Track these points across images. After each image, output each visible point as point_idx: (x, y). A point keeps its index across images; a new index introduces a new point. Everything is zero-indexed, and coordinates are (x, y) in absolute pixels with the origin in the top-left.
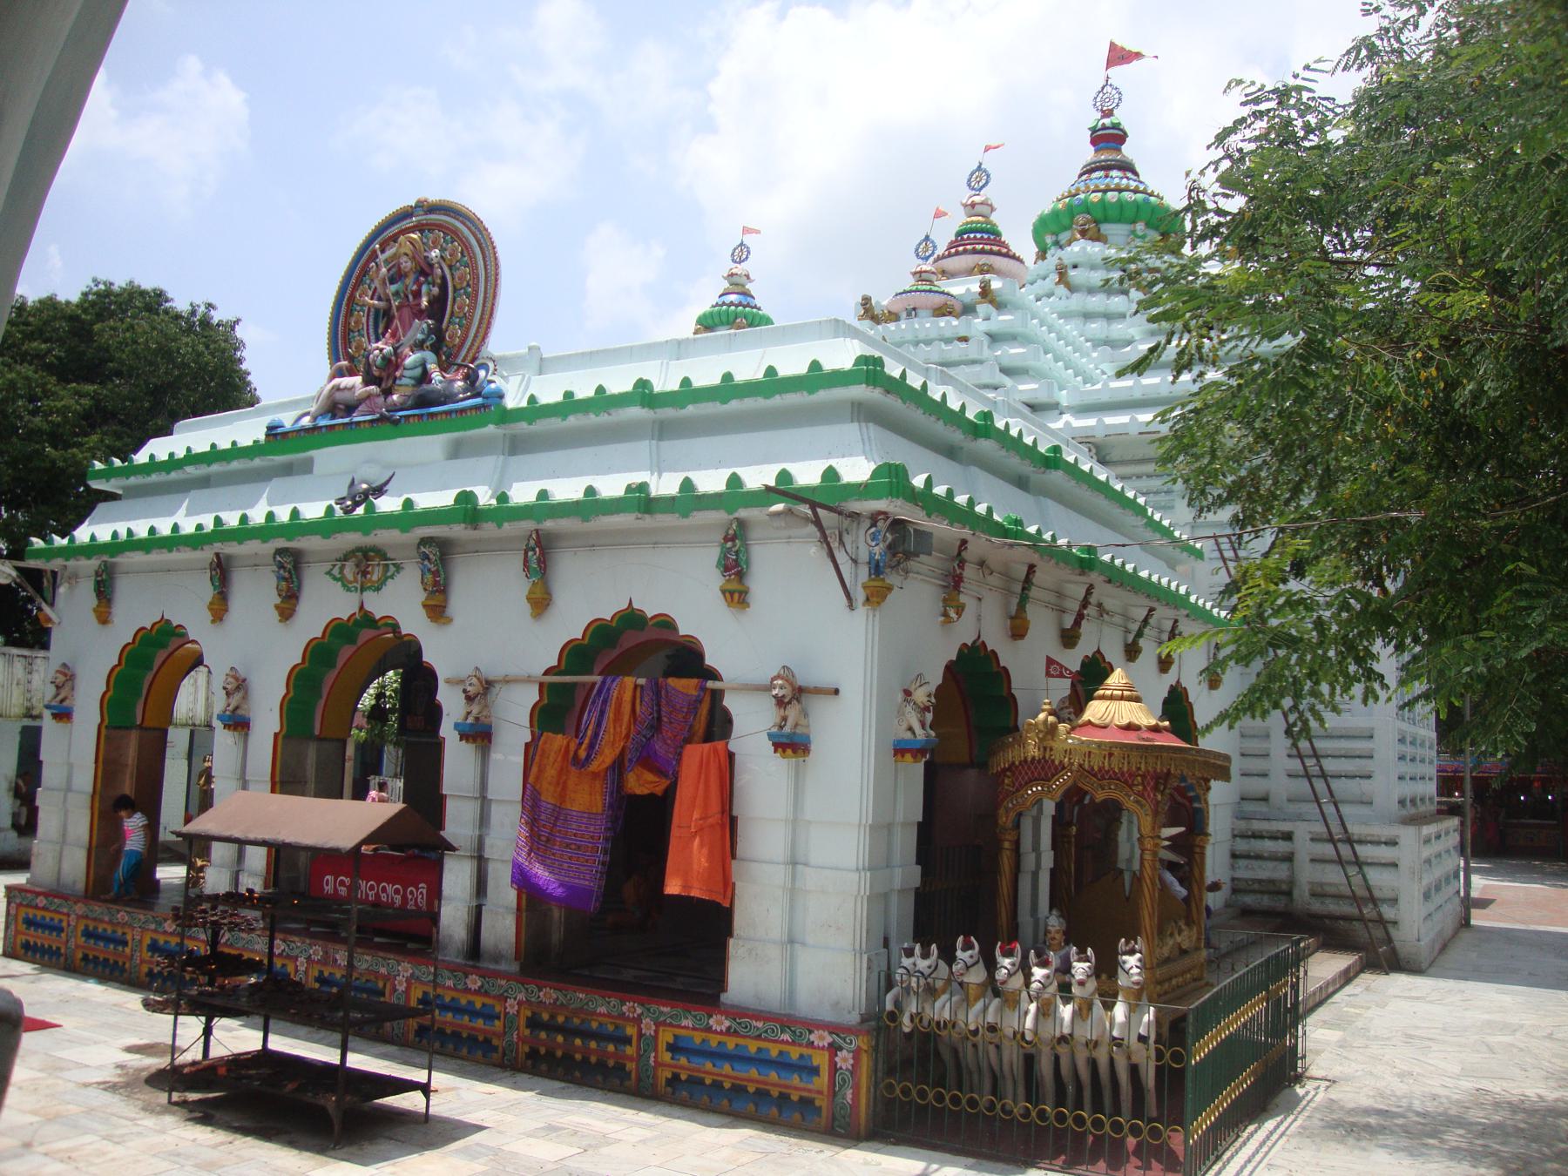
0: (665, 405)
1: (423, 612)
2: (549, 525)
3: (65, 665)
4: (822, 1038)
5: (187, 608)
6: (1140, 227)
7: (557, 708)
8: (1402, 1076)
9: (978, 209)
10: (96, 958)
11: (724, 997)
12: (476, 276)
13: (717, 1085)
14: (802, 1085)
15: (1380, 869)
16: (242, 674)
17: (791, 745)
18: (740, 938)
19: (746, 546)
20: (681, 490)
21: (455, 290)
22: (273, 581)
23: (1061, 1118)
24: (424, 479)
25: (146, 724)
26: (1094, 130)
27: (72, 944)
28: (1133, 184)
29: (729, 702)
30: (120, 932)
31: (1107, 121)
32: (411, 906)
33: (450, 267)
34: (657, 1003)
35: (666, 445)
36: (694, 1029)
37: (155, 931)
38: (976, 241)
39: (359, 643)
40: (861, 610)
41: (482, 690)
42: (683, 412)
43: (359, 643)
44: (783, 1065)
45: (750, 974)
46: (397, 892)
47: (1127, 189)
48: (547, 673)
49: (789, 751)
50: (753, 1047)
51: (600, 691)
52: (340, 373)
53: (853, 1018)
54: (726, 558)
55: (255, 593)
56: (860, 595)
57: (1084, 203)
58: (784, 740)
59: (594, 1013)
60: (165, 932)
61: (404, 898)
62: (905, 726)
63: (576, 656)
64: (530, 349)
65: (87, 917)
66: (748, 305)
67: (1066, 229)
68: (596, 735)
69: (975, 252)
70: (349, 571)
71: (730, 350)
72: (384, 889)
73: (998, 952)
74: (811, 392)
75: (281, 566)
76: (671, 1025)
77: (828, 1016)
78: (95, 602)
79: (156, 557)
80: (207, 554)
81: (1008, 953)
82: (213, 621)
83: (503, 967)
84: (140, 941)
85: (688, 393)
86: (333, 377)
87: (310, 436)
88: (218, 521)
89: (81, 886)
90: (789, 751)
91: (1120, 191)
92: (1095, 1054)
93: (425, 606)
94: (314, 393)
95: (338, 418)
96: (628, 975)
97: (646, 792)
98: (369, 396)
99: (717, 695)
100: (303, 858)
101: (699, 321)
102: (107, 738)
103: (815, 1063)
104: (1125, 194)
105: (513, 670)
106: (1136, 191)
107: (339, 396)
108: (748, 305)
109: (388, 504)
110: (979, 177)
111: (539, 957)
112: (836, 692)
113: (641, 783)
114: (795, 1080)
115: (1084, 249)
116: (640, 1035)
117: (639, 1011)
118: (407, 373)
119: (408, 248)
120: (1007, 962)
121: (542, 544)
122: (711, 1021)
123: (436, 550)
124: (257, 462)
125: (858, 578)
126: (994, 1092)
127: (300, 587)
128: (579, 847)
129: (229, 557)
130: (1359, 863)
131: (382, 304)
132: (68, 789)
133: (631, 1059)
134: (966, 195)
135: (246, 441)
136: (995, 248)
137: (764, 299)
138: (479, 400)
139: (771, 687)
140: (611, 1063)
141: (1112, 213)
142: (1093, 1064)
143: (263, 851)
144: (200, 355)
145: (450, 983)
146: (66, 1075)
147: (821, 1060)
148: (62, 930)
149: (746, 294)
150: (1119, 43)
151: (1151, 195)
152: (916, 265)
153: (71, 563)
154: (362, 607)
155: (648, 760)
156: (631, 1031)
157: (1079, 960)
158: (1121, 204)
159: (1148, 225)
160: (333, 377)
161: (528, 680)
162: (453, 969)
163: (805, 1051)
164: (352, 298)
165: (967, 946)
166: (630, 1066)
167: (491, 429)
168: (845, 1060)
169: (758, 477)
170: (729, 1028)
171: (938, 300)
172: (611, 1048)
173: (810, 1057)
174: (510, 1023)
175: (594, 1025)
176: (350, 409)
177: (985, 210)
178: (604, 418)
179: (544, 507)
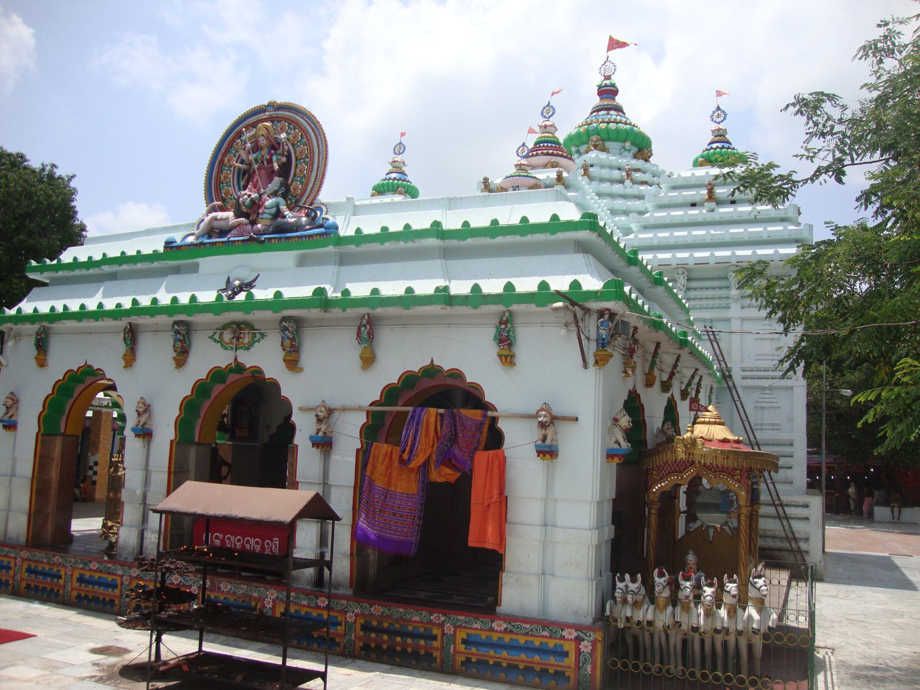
0: (449, 238)
1: (283, 364)
2: (379, 310)
3: (12, 393)
4: (570, 634)
5: (106, 357)
6: (628, 144)
7: (381, 426)
8: (867, 644)
9: (548, 129)
10: (36, 587)
11: (498, 609)
12: (312, 152)
13: (544, 672)
14: (557, 663)
15: (798, 521)
16: (148, 402)
17: (547, 452)
18: (510, 572)
19: (513, 327)
20: (472, 292)
21: (297, 159)
22: (171, 342)
23: (704, 676)
24: (282, 279)
26: (600, 87)
27: (18, 577)
28: (624, 120)
29: (501, 425)
30: (55, 569)
31: (608, 82)
32: (267, 552)
33: (293, 145)
34: (455, 614)
35: (450, 263)
36: (482, 630)
37: (83, 569)
38: (547, 148)
39: (227, 383)
40: (592, 369)
41: (326, 415)
42: (464, 243)
43: (227, 383)
44: (542, 651)
45: (516, 594)
46: (257, 543)
47: (620, 122)
48: (371, 405)
49: (548, 456)
50: (522, 640)
51: (413, 417)
52: (213, 209)
53: (589, 621)
54: (500, 334)
55: (156, 351)
56: (591, 360)
57: (596, 128)
58: (547, 449)
59: (411, 621)
60: (90, 570)
61: (263, 547)
62: (614, 440)
63: (391, 394)
64: (347, 199)
65: (30, 560)
66: (405, 180)
67: (584, 143)
68: (413, 444)
69: (548, 154)
70: (227, 336)
72: (248, 542)
73: (680, 578)
74: (552, 234)
75: (177, 332)
76: (465, 627)
77: (571, 620)
78: (35, 353)
79: (84, 324)
80: (123, 323)
81: (687, 579)
82: (125, 367)
83: (341, 591)
84: (71, 576)
85: (467, 231)
86: (209, 212)
87: (198, 249)
88: (135, 302)
89: (23, 539)
90: (548, 456)
91: (617, 123)
92: (727, 638)
93: (284, 360)
94: (196, 220)
95: (214, 238)
96: (422, 595)
97: (444, 480)
98: (239, 225)
99: (494, 420)
100: (187, 521)
101: (375, 188)
102: (42, 442)
104: (611, 125)
105: (348, 403)
106: (626, 123)
107: (216, 224)
108: (405, 180)
109: (262, 294)
110: (548, 110)
111: (365, 586)
112: (577, 419)
113: (442, 475)
114: (552, 660)
115: (597, 156)
116: (443, 634)
117: (442, 619)
118: (266, 211)
119: (264, 132)
120: (688, 584)
121: (369, 324)
122: (494, 625)
123: (293, 325)
124: (156, 264)
125: (591, 349)
126: (662, 662)
127: (190, 346)
128: (402, 516)
129: (137, 325)
130: (787, 518)
131: (243, 166)
133: (436, 649)
134: (541, 121)
135: (147, 251)
136: (560, 153)
137: (414, 178)
138: (322, 230)
139: (536, 416)
140: (422, 652)
142: (725, 644)
144: (50, 196)
145: (305, 602)
146: (61, 671)
147: (570, 647)
148: (10, 568)
149: (403, 173)
150: (615, 37)
151: (634, 126)
152: (517, 160)
153: (20, 326)
154: (236, 359)
155: (447, 459)
156: (436, 631)
157: (730, 582)
158: (618, 131)
159: (632, 144)
160: (209, 212)
161: (360, 409)
162: (307, 593)
163: (559, 642)
164: (222, 162)
165: (661, 575)
166: (436, 654)
167: (330, 248)
168: (586, 647)
169: (526, 285)
171: (532, 181)
172: (422, 642)
173: (561, 646)
174: (349, 627)
175: (410, 628)
176: (223, 232)
177: (552, 129)
178: (410, 244)
179: (375, 299)
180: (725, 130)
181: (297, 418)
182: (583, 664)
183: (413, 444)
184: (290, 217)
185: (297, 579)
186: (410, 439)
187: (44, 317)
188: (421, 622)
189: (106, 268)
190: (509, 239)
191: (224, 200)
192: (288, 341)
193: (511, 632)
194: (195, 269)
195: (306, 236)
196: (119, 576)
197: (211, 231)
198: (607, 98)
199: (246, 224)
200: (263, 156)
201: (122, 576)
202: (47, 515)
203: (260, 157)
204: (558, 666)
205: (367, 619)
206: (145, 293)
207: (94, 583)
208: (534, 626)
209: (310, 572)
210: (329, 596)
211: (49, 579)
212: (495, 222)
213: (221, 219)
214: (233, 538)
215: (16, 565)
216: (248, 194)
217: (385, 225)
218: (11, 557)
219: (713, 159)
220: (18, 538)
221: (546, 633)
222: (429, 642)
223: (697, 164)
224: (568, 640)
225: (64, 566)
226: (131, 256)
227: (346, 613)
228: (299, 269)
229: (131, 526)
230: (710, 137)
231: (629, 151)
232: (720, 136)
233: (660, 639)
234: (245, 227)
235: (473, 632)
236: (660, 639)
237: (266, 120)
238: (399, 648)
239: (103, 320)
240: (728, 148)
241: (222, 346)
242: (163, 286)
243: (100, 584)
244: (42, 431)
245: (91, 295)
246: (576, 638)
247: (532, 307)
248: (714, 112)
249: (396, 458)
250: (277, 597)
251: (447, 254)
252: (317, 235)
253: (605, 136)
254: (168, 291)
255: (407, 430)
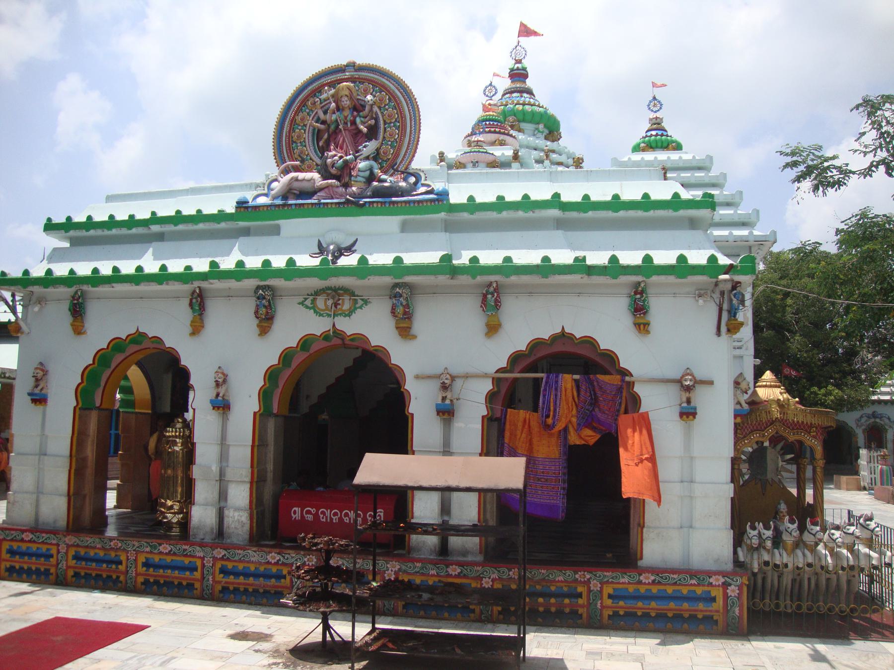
1: (396, 332)
3: (41, 364)
4: (717, 580)
6: (541, 126)
11: (640, 563)
17: (688, 414)
18: (649, 527)
20: (609, 262)
21: (385, 123)
24: (383, 245)
25: (103, 406)
26: (512, 70)
27: (63, 565)
29: (637, 389)
30: (113, 554)
31: (520, 66)
33: (380, 108)
36: (629, 583)
44: (692, 598)
48: (496, 372)
49: (691, 417)
50: (670, 590)
52: (286, 172)
57: (513, 109)
59: (554, 581)
60: (161, 553)
66: (667, 136)
68: (555, 410)
69: (495, 132)
71: (588, 181)
72: (347, 515)
76: (612, 583)
77: (714, 568)
79: (143, 288)
82: (260, 335)
83: (470, 558)
85: (586, 204)
89: (62, 523)
91: (524, 104)
95: (295, 201)
97: (583, 442)
99: (631, 385)
103: (713, 595)
104: (527, 107)
105: (471, 370)
107: (296, 185)
109: (349, 261)
114: (701, 606)
116: (589, 591)
117: (588, 576)
118: (361, 174)
121: (492, 292)
124: (223, 225)
128: (547, 480)
132: (43, 453)
133: (582, 606)
135: (210, 209)
141: (528, 117)
143: (435, 497)
145: (434, 572)
147: (717, 593)
154: (334, 325)
158: (533, 113)
159: (545, 126)
161: (486, 376)
163: (706, 588)
168: (733, 591)
169: (664, 257)
170: (654, 581)
171: (491, 158)
173: (709, 592)
175: (553, 588)
178: (530, 214)
179: (508, 268)
180: (662, 119)
181: (410, 385)
182: (731, 607)
183: (555, 410)
184: (389, 180)
185: (418, 549)
186: (552, 404)
187: (84, 280)
188: (566, 581)
189: (155, 228)
190: (632, 213)
191: (303, 161)
192: (401, 308)
193: (659, 583)
194: (276, 231)
195: (414, 202)
196: (200, 557)
197: (288, 193)
198: (519, 81)
199: (337, 187)
200: (346, 118)
201: (203, 559)
202: (85, 496)
203: (342, 117)
204: (706, 611)
205: (505, 583)
206: (256, 253)
207: (165, 567)
208: (681, 576)
209: (432, 540)
210: (460, 564)
211: (105, 565)
212: (616, 197)
213: (304, 180)
214: (328, 513)
215: (58, 552)
216: (334, 156)
217: (501, 194)
218: (51, 544)
219: (654, 145)
220: (55, 522)
221: (694, 582)
222: (573, 600)
223: (636, 149)
224: (715, 586)
225: (124, 550)
226: (190, 216)
227: (481, 579)
228: (404, 234)
229: (206, 505)
230: (648, 126)
231: (542, 132)
232: (657, 125)
233: (772, 581)
234: (336, 190)
235: (620, 586)
236: (772, 581)
237: (346, 80)
238: (541, 609)
239: (167, 284)
240: (662, 135)
241: (315, 312)
242: (236, 247)
243: (174, 568)
244: (80, 406)
245: (228, 253)
246: (723, 583)
247: (671, 279)
248: (651, 102)
249: (534, 424)
250: (400, 570)
251: (560, 224)
252: (427, 201)
253: (521, 117)
254: (156, 257)
255: (544, 396)
